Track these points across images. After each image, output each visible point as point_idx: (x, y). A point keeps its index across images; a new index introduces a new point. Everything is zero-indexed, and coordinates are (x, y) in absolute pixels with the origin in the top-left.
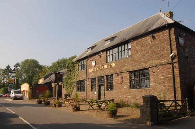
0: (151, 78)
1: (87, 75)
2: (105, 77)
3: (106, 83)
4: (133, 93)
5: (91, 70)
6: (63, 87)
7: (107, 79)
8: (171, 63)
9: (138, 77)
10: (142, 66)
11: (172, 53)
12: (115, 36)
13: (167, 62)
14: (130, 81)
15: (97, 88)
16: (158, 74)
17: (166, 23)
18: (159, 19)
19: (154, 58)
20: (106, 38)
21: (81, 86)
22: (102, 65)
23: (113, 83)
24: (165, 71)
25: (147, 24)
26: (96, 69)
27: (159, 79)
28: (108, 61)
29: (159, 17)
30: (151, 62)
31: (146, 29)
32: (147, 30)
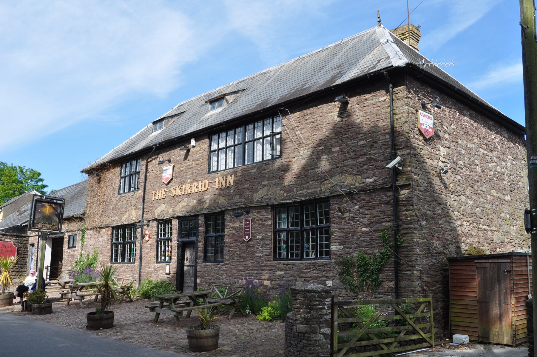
0: (334, 228)
1: (143, 209)
2: (201, 221)
3: (201, 238)
4: (281, 273)
5: (160, 193)
6: (65, 245)
7: (207, 226)
8: (391, 187)
9: (297, 225)
10: (309, 191)
11: (395, 156)
12: (241, 87)
13: (380, 182)
14: (276, 232)
15: (175, 251)
16: (353, 218)
17: (383, 65)
18: (370, 49)
19: (345, 168)
20: (214, 91)
21: (452, 202)
22: (194, 180)
23: (222, 237)
24: (375, 212)
25: (336, 61)
26: (175, 189)
27: (355, 233)
28: (214, 168)
29: (374, 43)
30: (335, 180)
31: (329, 77)
32: (334, 78)
